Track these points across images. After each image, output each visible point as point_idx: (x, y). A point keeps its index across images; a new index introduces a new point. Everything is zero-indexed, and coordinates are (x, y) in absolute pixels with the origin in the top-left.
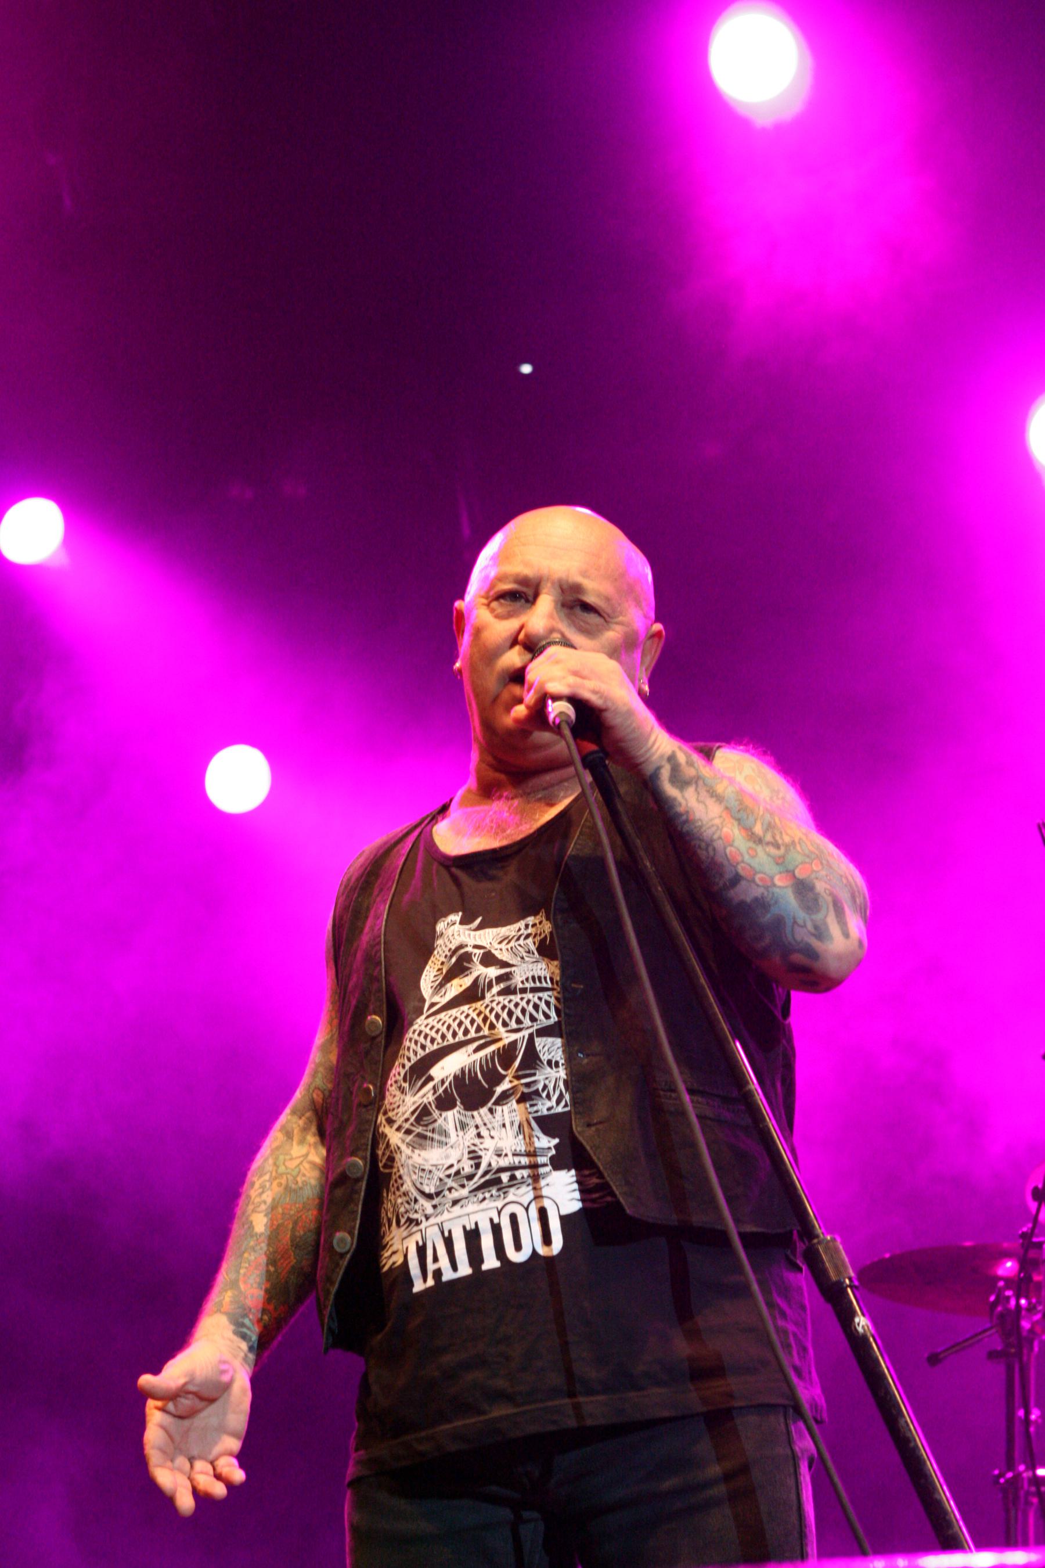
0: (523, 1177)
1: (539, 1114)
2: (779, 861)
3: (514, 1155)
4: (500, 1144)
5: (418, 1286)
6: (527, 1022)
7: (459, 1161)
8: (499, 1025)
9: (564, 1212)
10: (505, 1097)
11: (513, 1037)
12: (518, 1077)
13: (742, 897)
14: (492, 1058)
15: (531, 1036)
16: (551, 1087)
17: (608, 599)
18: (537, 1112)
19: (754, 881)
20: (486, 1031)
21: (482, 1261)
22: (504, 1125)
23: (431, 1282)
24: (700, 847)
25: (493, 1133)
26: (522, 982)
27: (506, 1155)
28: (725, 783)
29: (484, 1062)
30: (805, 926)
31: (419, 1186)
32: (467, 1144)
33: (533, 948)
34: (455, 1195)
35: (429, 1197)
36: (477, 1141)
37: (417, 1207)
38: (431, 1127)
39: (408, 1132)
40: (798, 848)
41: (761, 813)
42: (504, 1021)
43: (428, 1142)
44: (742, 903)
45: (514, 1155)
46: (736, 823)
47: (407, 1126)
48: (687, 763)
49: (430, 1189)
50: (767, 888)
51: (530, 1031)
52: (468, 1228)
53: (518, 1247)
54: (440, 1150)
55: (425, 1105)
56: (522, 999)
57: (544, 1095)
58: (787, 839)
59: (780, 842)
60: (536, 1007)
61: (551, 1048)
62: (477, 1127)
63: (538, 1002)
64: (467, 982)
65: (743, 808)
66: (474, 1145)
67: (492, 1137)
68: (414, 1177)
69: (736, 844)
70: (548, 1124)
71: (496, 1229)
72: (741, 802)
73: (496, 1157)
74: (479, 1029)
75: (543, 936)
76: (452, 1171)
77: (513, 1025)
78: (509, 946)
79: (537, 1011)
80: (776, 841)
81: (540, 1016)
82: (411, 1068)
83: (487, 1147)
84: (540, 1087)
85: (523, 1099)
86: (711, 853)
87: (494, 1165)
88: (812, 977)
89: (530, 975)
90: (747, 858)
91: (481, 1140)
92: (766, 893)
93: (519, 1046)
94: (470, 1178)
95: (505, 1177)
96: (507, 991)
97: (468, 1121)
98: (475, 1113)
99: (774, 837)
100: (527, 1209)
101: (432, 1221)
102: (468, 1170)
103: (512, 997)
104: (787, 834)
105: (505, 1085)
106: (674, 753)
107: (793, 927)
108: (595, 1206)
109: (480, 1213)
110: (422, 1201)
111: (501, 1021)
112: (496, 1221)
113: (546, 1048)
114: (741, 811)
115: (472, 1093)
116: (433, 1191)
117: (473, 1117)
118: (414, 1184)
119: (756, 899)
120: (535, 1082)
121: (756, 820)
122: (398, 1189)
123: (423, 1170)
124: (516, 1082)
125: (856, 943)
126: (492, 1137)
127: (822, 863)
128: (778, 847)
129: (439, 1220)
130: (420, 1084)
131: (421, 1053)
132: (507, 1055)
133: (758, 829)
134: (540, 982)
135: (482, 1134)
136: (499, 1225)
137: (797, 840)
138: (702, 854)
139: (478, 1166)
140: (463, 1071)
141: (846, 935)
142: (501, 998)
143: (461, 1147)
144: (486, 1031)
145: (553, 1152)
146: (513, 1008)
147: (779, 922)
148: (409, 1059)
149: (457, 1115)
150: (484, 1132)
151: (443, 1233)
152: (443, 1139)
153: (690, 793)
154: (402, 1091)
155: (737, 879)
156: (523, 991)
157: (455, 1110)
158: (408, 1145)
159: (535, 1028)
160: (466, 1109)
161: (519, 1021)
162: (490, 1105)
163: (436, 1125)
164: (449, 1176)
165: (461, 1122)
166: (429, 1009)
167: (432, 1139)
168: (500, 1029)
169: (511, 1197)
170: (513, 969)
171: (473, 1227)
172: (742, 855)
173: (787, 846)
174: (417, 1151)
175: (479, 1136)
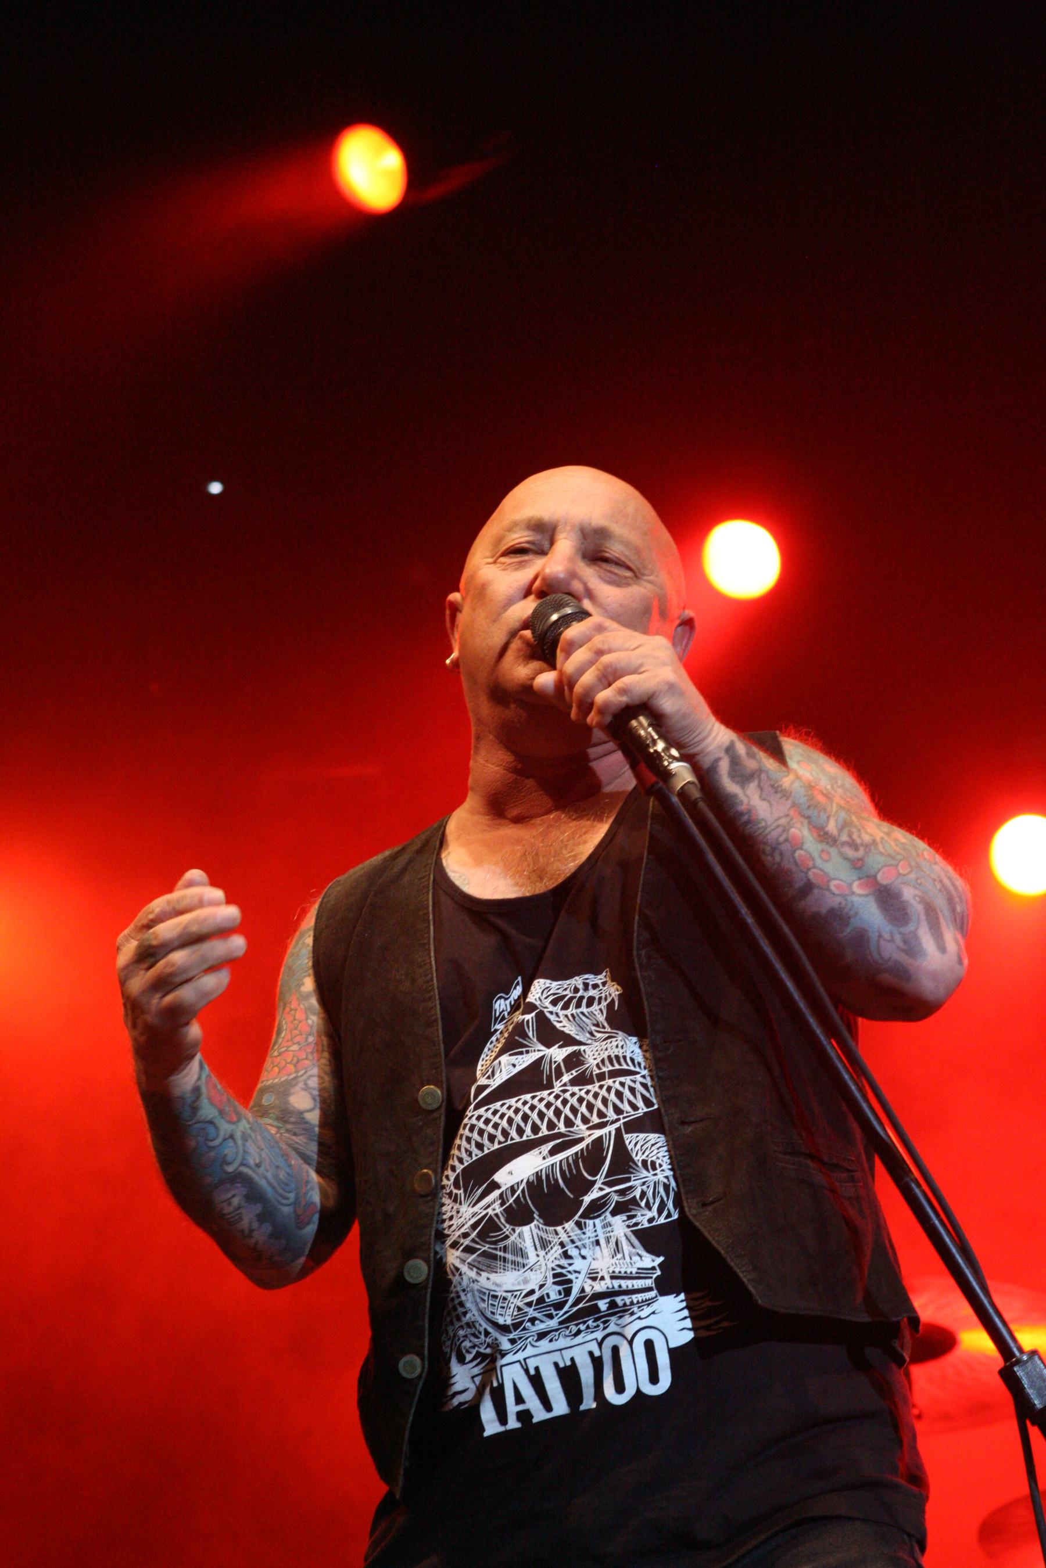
0: (625, 1305)
1: (639, 1227)
2: (857, 865)
3: (612, 1278)
4: (595, 1265)
5: (491, 1426)
6: (611, 1115)
7: (541, 1286)
8: (578, 1121)
9: (672, 1346)
10: (596, 1208)
11: (598, 1133)
13: (814, 909)
14: (576, 1162)
15: (618, 1130)
16: (650, 1194)
17: (638, 551)
18: (636, 1224)
19: (828, 889)
20: (562, 1128)
21: (581, 1401)
22: (598, 1243)
23: (513, 1424)
24: (764, 852)
25: (584, 1252)
26: (598, 1066)
27: (603, 1278)
28: (791, 777)
29: (565, 1167)
30: (892, 941)
31: (489, 1315)
32: (550, 1265)
33: (602, 1018)
34: (540, 1327)
35: (504, 1329)
36: (564, 1262)
38: (501, 1245)
39: (469, 1250)
40: (880, 847)
41: (834, 810)
44: (816, 916)
45: (612, 1278)
46: (806, 822)
47: (467, 1242)
48: (748, 754)
50: (844, 896)
51: (617, 1125)
52: (562, 1365)
53: (620, 1388)
54: (516, 1273)
56: (601, 1087)
57: (643, 1204)
58: (867, 838)
59: (859, 841)
60: (619, 1095)
61: (651, 1148)
62: (562, 1245)
63: (620, 1088)
64: (524, 1061)
65: (812, 805)
66: (562, 1267)
67: (584, 1257)
68: (483, 1305)
69: (805, 847)
70: (649, 1239)
71: (597, 1363)
72: (811, 798)
73: (590, 1282)
74: (551, 1126)
75: (609, 1000)
76: (534, 1298)
77: (595, 1120)
78: (568, 1012)
79: (622, 1101)
80: (853, 841)
81: (626, 1107)
82: (463, 1170)
83: (577, 1269)
84: (637, 1194)
85: (620, 1209)
86: (778, 858)
87: (588, 1289)
88: (900, 1001)
89: (605, 1055)
90: (819, 862)
91: (570, 1261)
92: (844, 902)
93: (606, 1146)
94: (559, 1306)
95: (603, 1305)
96: (581, 1080)
97: (550, 1237)
98: (559, 1228)
99: (850, 835)
100: (631, 1343)
102: (554, 1296)
103: (589, 1087)
104: (867, 833)
105: (594, 1194)
106: (732, 743)
107: (878, 941)
108: (712, 1333)
109: (580, 1349)
110: (495, 1333)
112: (597, 1353)
114: (810, 810)
115: (550, 1203)
116: (509, 1322)
117: (557, 1234)
118: (483, 1314)
119: (832, 911)
120: (631, 1188)
121: (828, 817)
122: (459, 1319)
123: (496, 1297)
124: (608, 1190)
125: (955, 958)
126: (584, 1257)
127: (910, 866)
128: (855, 847)
129: (520, 1356)
130: (480, 1191)
131: (477, 1154)
132: (594, 1155)
133: (832, 827)
134: (620, 1064)
135: (569, 1253)
136: (600, 1358)
137: (878, 839)
138: (768, 860)
139: (568, 1292)
140: (538, 1175)
141: (942, 949)
142: (576, 1089)
143: (543, 1269)
144: (562, 1128)
145: (659, 1273)
146: (592, 1100)
147: (861, 937)
148: (461, 1161)
149: (535, 1231)
150: (573, 1252)
151: (527, 1371)
152: (519, 1259)
153: (752, 787)
154: (456, 1199)
155: (808, 887)
156: (601, 1077)
157: (532, 1225)
158: (471, 1266)
159: (622, 1121)
160: (547, 1223)
161: (601, 1115)
162: (576, 1218)
163: (508, 1242)
164: (529, 1304)
165: (541, 1239)
166: (475, 1098)
168: (580, 1128)
169: (612, 1328)
170: (582, 1048)
171: (568, 1363)
172: (813, 859)
173: (867, 846)
174: (484, 1274)
175: (566, 1255)
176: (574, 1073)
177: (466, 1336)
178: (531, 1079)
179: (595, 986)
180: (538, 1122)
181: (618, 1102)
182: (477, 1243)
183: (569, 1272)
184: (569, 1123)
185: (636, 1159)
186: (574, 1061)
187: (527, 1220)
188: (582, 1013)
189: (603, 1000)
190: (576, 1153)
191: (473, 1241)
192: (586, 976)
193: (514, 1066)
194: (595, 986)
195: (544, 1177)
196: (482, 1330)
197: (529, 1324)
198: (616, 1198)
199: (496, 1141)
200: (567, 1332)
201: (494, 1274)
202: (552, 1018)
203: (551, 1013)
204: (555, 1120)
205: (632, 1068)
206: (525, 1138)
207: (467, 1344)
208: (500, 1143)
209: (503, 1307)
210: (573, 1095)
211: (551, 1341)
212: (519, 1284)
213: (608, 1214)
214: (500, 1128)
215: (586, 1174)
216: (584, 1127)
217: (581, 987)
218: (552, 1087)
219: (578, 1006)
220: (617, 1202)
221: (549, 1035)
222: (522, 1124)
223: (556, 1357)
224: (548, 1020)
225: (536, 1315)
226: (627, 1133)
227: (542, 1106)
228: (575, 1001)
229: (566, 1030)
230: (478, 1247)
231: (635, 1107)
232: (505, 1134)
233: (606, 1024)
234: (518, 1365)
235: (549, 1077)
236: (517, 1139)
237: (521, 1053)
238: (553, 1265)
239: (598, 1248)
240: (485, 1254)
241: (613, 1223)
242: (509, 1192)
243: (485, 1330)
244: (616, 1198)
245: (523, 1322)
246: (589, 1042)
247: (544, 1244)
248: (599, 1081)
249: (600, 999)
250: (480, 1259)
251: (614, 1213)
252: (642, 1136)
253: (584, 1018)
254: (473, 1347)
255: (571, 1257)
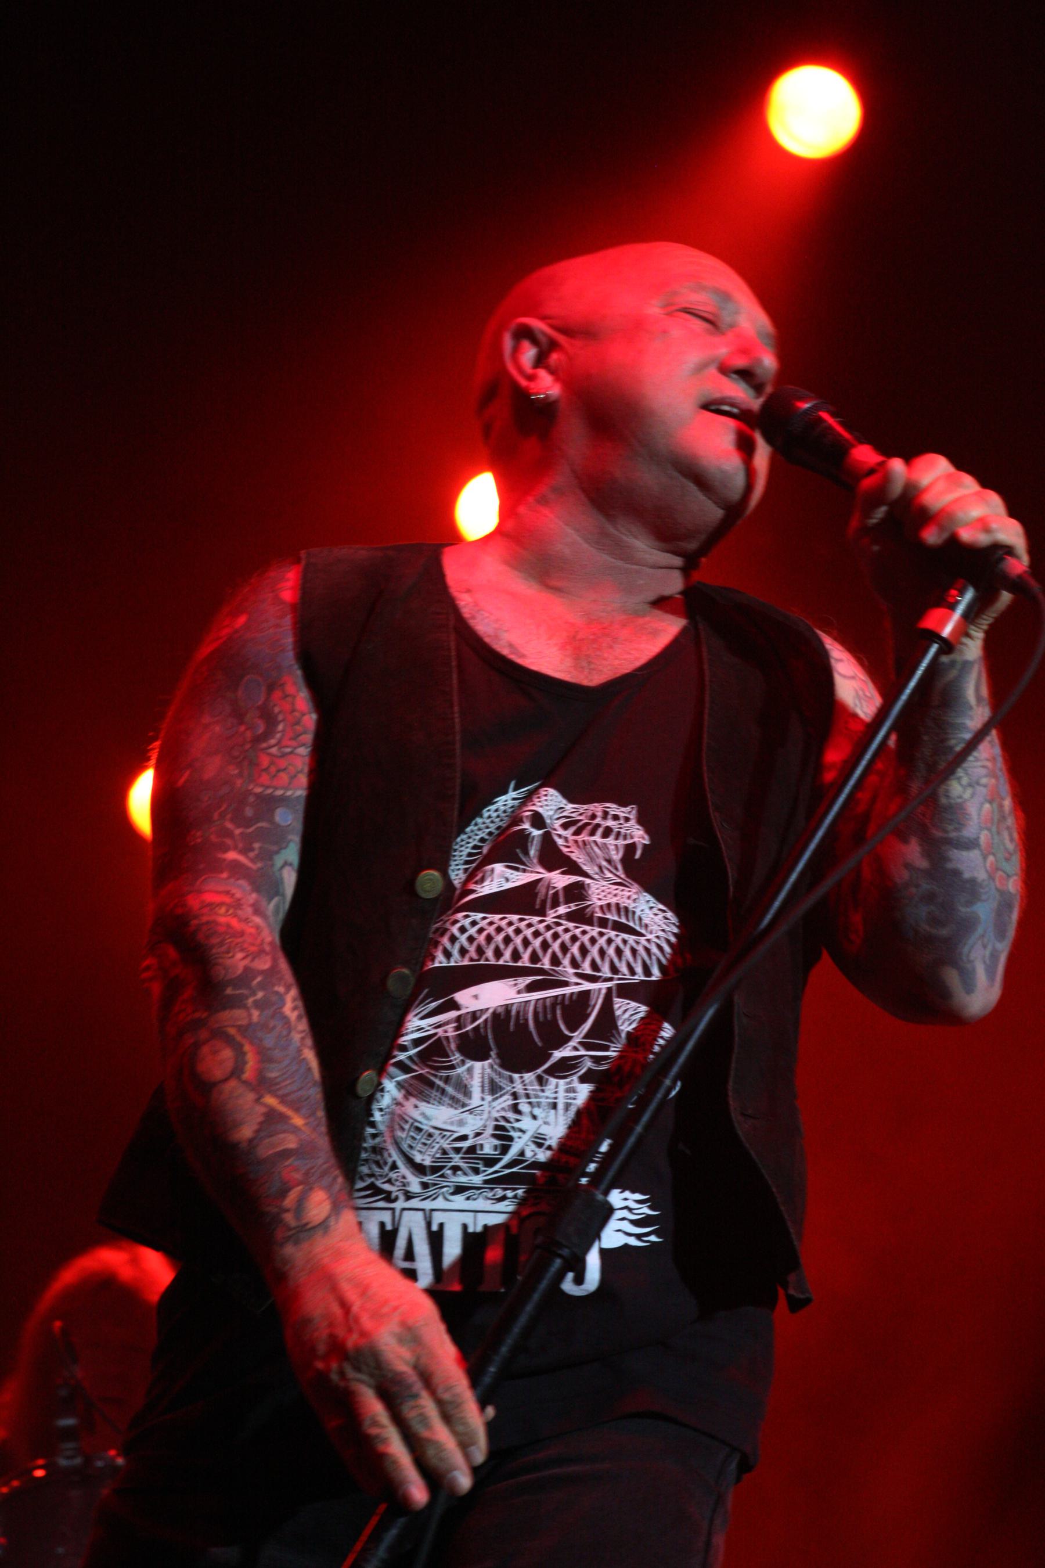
4: (544, 1130)
6: (606, 972)
7: (478, 1134)
8: (566, 962)
10: (563, 1068)
11: (587, 986)
12: (588, 1047)
14: (545, 1007)
15: (609, 989)
20: (546, 963)
22: (554, 1106)
25: (537, 1111)
29: (540, 1010)
33: (617, 857)
34: (462, 1179)
35: (419, 1169)
36: (511, 1115)
37: (393, 1175)
38: (444, 1073)
42: (554, 954)
43: (434, 1093)
49: (425, 1159)
51: (609, 984)
52: (471, 1230)
55: (439, 1039)
56: (601, 934)
60: (619, 952)
62: (515, 1096)
63: (621, 946)
64: (519, 879)
67: (534, 1117)
73: (533, 1147)
74: (535, 958)
76: (465, 1144)
78: (580, 838)
81: (624, 969)
83: (524, 1128)
87: (529, 1154)
89: (614, 901)
91: (518, 1117)
93: (593, 1003)
94: (490, 1162)
96: (580, 917)
97: (503, 1083)
98: (516, 1076)
101: (414, 1203)
103: (587, 928)
110: (404, 1169)
111: (569, 955)
113: (626, 1015)
115: (518, 1046)
116: (428, 1162)
123: (419, 1130)
124: (583, 1052)
126: (534, 1117)
129: (428, 1205)
130: (434, 1005)
139: (505, 1150)
140: (507, 1008)
142: (571, 925)
143: (485, 1116)
144: (546, 963)
146: (588, 944)
149: (488, 1071)
150: (524, 1107)
151: (429, 1224)
152: (460, 1096)
156: (603, 923)
157: (486, 1063)
160: (504, 1065)
161: (594, 966)
162: (539, 1071)
163: (453, 1073)
164: (457, 1150)
167: (443, 1092)
168: (567, 969)
170: (588, 881)
174: (413, 1100)
176: (573, 907)
177: (366, 1161)
178: (523, 900)
179: (616, 818)
180: (521, 948)
181: (616, 960)
182: (416, 1064)
183: (513, 1128)
184: (555, 961)
185: (621, 1028)
186: (575, 892)
187: (482, 1057)
188: (595, 842)
189: (621, 838)
190: (557, 996)
191: (410, 1058)
192: (608, 805)
193: (507, 880)
194: (616, 818)
195: (514, 1012)
196: (390, 1161)
197: (449, 1172)
198: (589, 1064)
199: (467, 957)
200: (490, 1195)
201: (424, 1104)
202: (560, 842)
203: (560, 836)
204: (540, 953)
205: (638, 928)
206: (501, 962)
207: (365, 1170)
208: (472, 960)
209: (425, 1144)
210: (567, 930)
211: (468, 1198)
212: (452, 1123)
213: (575, 1078)
214: (475, 944)
215: (563, 1027)
216: (571, 971)
217: (599, 814)
218: (545, 915)
219: (592, 833)
220: (589, 1070)
221: (553, 857)
222: (502, 946)
223: (468, 1218)
224: (554, 843)
225: (461, 1164)
226: (619, 997)
227: (528, 933)
228: (589, 827)
229: (573, 856)
230: (415, 1067)
231: (633, 972)
232: (480, 951)
233: (620, 867)
234: (420, 1214)
235: (544, 902)
236: (493, 962)
237: (517, 869)
238: (497, 1115)
239: (553, 1111)
240: (420, 1078)
241: (578, 1090)
242: (469, 1018)
243: (394, 1163)
244: (589, 1064)
245: (444, 1167)
246: (596, 877)
247: (494, 1089)
248: (600, 926)
249: (619, 833)
250: (413, 1082)
251: (583, 1080)
252: (633, 1004)
253: (596, 849)
254: (372, 1175)
255: (519, 1112)
